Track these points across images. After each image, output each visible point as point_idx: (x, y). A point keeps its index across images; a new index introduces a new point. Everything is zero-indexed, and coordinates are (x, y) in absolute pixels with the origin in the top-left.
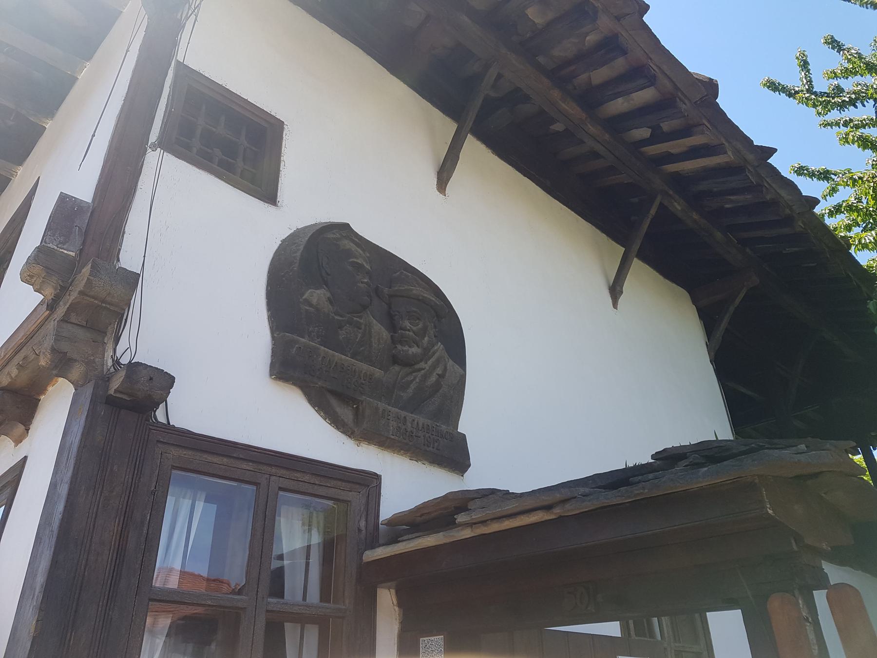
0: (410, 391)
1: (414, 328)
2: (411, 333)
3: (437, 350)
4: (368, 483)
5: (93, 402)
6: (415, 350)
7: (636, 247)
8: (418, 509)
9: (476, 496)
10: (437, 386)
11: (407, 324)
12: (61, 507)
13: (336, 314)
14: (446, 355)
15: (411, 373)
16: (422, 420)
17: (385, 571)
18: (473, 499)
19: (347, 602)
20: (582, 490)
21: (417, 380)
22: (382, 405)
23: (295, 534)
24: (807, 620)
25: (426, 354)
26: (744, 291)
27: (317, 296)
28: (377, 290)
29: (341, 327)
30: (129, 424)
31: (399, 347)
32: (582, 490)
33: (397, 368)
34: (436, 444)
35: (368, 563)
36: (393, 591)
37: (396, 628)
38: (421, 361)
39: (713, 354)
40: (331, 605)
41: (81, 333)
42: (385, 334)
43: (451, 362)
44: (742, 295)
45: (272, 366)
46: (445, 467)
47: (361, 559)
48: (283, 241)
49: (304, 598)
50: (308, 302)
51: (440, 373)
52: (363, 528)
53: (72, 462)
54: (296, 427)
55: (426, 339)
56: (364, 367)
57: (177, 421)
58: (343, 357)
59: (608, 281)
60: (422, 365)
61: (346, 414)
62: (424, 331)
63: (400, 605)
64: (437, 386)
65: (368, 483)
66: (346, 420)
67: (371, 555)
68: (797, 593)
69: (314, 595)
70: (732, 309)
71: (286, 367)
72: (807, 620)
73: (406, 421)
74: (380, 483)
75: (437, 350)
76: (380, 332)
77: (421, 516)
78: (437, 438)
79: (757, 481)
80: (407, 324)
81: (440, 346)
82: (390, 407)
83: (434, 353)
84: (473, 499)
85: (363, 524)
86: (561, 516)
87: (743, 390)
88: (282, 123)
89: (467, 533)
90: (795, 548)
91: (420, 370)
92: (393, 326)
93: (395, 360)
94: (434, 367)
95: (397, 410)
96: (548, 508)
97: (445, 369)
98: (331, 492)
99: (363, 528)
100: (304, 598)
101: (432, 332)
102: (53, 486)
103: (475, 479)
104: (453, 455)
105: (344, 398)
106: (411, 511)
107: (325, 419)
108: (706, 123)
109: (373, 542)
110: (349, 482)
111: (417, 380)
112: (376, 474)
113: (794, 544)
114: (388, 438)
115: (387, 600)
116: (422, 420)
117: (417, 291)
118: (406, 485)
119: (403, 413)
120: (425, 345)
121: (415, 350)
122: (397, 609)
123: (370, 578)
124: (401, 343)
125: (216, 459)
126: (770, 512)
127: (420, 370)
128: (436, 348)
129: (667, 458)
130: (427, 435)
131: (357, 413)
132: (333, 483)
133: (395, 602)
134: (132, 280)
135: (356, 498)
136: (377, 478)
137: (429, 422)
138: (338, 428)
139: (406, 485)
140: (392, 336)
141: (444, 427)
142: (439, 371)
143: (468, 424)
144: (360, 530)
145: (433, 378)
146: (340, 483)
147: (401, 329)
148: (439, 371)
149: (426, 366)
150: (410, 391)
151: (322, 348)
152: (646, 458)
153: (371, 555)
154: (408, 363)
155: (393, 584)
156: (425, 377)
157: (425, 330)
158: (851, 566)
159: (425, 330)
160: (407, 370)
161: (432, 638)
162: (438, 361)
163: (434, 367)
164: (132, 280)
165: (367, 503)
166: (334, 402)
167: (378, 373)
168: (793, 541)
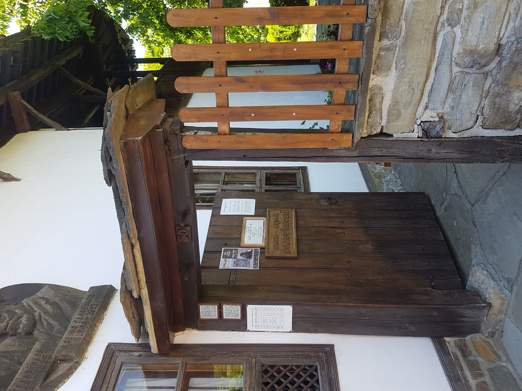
1: (7, 319)
2: (11, 322)
3: (27, 303)
4: (112, 351)
6: (24, 320)
8: (129, 320)
9: (124, 285)
10: (54, 305)
14: (33, 297)
15: (41, 322)
16: (76, 316)
17: (163, 338)
18: (126, 287)
19: (178, 362)
20: (123, 227)
21: (47, 318)
22: (61, 343)
24: (196, 133)
25: (29, 311)
26: (23, 101)
31: (20, 331)
32: (123, 227)
33: (36, 332)
34: (94, 306)
35: (159, 350)
36: (176, 334)
38: (33, 315)
39: (63, 128)
40: (179, 371)
42: (8, 341)
43: (38, 294)
44: (26, 103)
45: (115, 344)
46: (110, 301)
47: (156, 354)
49: (173, 388)
51: (45, 302)
52: (139, 353)
55: (17, 311)
56: (31, 355)
58: (19, 371)
60: (36, 315)
61: (63, 367)
62: (11, 313)
63: (184, 330)
64: (54, 305)
66: (68, 368)
67: (154, 348)
68: (183, 134)
70: (34, 111)
72: (196, 133)
73: (75, 327)
74: (113, 343)
75: (27, 303)
77: (134, 317)
78: (89, 306)
79: (123, 141)
81: (25, 302)
82: (64, 338)
83: (29, 305)
84: (126, 287)
85: (136, 354)
86: (138, 239)
87: (91, 115)
89: (145, 293)
90: (161, 130)
91: (40, 316)
93: (30, 333)
94: (39, 306)
95: (66, 333)
96: (133, 246)
97: (43, 298)
98: (114, 375)
99: (139, 353)
100: (173, 388)
101: (12, 307)
103: (117, 285)
104: (102, 296)
106: (131, 324)
107: (65, 382)
109: (146, 347)
110: (109, 364)
111: (47, 318)
112: (108, 345)
113: (159, 130)
114: (84, 339)
118: (115, 327)
119: (69, 328)
120: (22, 312)
121: (24, 320)
122: (185, 331)
123: (168, 349)
124: (16, 329)
126: (140, 138)
127: (40, 316)
128: (25, 304)
130: (87, 312)
131: (63, 361)
132: (109, 375)
133: (182, 332)
135: (121, 357)
138: (72, 373)
139: (115, 327)
140: (11, 336)
141: (83, 301)
142: (43, 303)
143: (84, 285)
144: (140, 356)
145: (48, 307)
146: (109, 370)
147: (6, 329)
148: (43, 303)
149: (37, 311)
151: (9, 388)
152: (109, 190)
154: (33, 324)
155: (171, 334)
156: (46, 313)
157: (10, 312)
159: (10, 312)
160: (38, 325)
161: (201, 311)
162: (36, 303)
163: (39, 306)
165: (125, 351)
166: (53, 377)
167: (37, 346)
168: (158, 130)
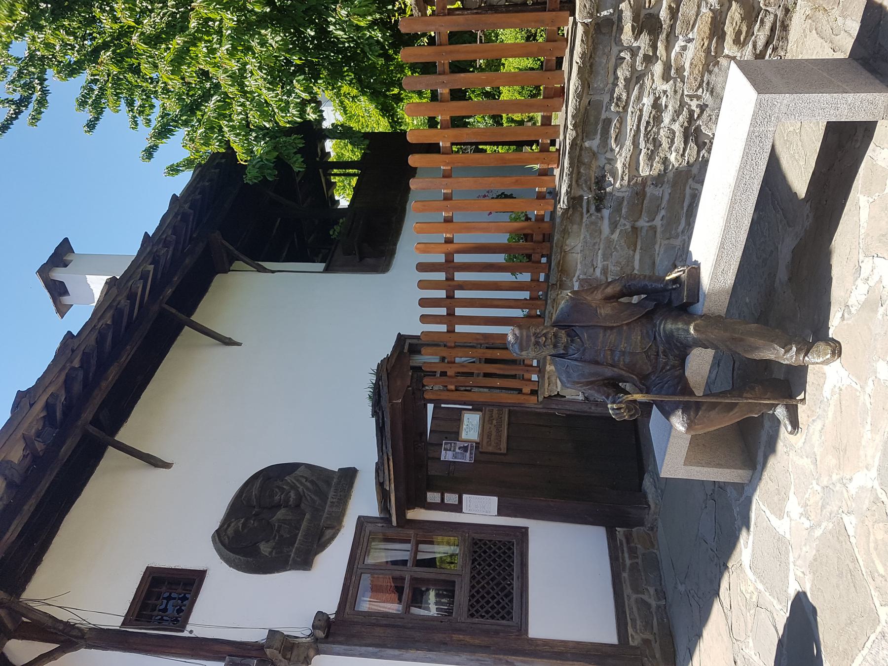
0: (316, 498)
5: (327, 643)
6: (292, 494)
7: (183, 317)
10: (312, 482)
11: (277, 498)
12: (370, 649)
13: (275, 538)
17: (401, 514)
22: (325, 515)
23: (381, 554)
25: (293, 487)
26: (224, 242)
27: (265, 548)
28: (256, 515)
29: (282, 536)
30: (333, 630)
31: (290, 503)
33: (302, 505)
37: (423, 511)
41: (295, 652)
48: (230, 566)
50: (270, 553)
53: (353, 647)
54: (335, 558)
56: (304, 524)
57: (335, 610)
59: (217, 345)
60: (300, 490)
61: (329, 533)
65: (362, 522)
67: (394, 523)
69: (407, 546)
71: (305, 562)
76: (281, 514)
80: (277, 498)
85: (380, 525)
88: (148, 568)
89: (393, 486)
92: (278, 506)
93: (298, 506)
94: (301, 483)
102: (361, 655)
105: (322, 534)
108: (130, 283)
109: (388, 520)
115: (412, 514)
116: (331, 493)
117: (255, 492)
118: (364, 502)
119: (329, 503)
121: (292, 494)
125: (350, 593)
129: (375, 413)
131: (327, 528)
134: (272, 633)
135: (369, 528)
136: (359, 517)
137: (332, 489)
142: (304, 480)
145: (308, 484)
148: (304, 480)
149: (301, 488)
150: (316, 498)
153: (394, 523)
154: (300, 498)
156: (308, 489)
158: (406, 202)
160: (304, 499)
163: (301, 483)
164: (272, 633)
166: (324, 539)
167: (307, 516)
